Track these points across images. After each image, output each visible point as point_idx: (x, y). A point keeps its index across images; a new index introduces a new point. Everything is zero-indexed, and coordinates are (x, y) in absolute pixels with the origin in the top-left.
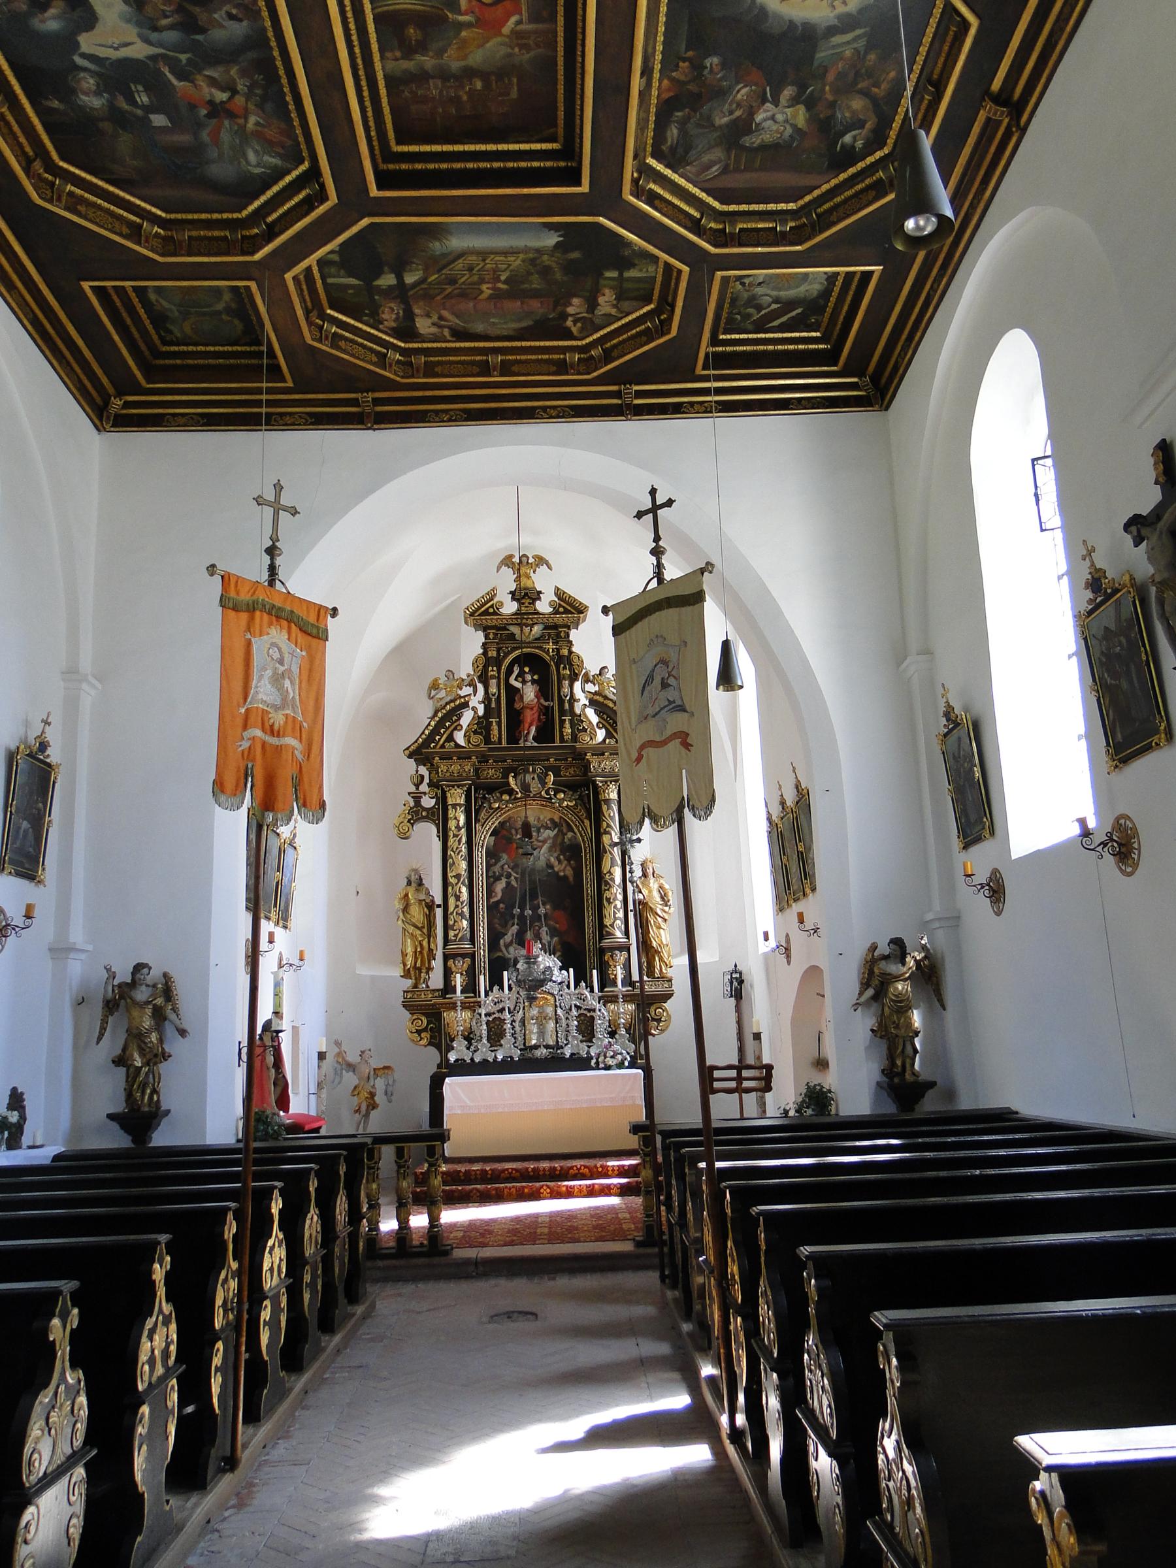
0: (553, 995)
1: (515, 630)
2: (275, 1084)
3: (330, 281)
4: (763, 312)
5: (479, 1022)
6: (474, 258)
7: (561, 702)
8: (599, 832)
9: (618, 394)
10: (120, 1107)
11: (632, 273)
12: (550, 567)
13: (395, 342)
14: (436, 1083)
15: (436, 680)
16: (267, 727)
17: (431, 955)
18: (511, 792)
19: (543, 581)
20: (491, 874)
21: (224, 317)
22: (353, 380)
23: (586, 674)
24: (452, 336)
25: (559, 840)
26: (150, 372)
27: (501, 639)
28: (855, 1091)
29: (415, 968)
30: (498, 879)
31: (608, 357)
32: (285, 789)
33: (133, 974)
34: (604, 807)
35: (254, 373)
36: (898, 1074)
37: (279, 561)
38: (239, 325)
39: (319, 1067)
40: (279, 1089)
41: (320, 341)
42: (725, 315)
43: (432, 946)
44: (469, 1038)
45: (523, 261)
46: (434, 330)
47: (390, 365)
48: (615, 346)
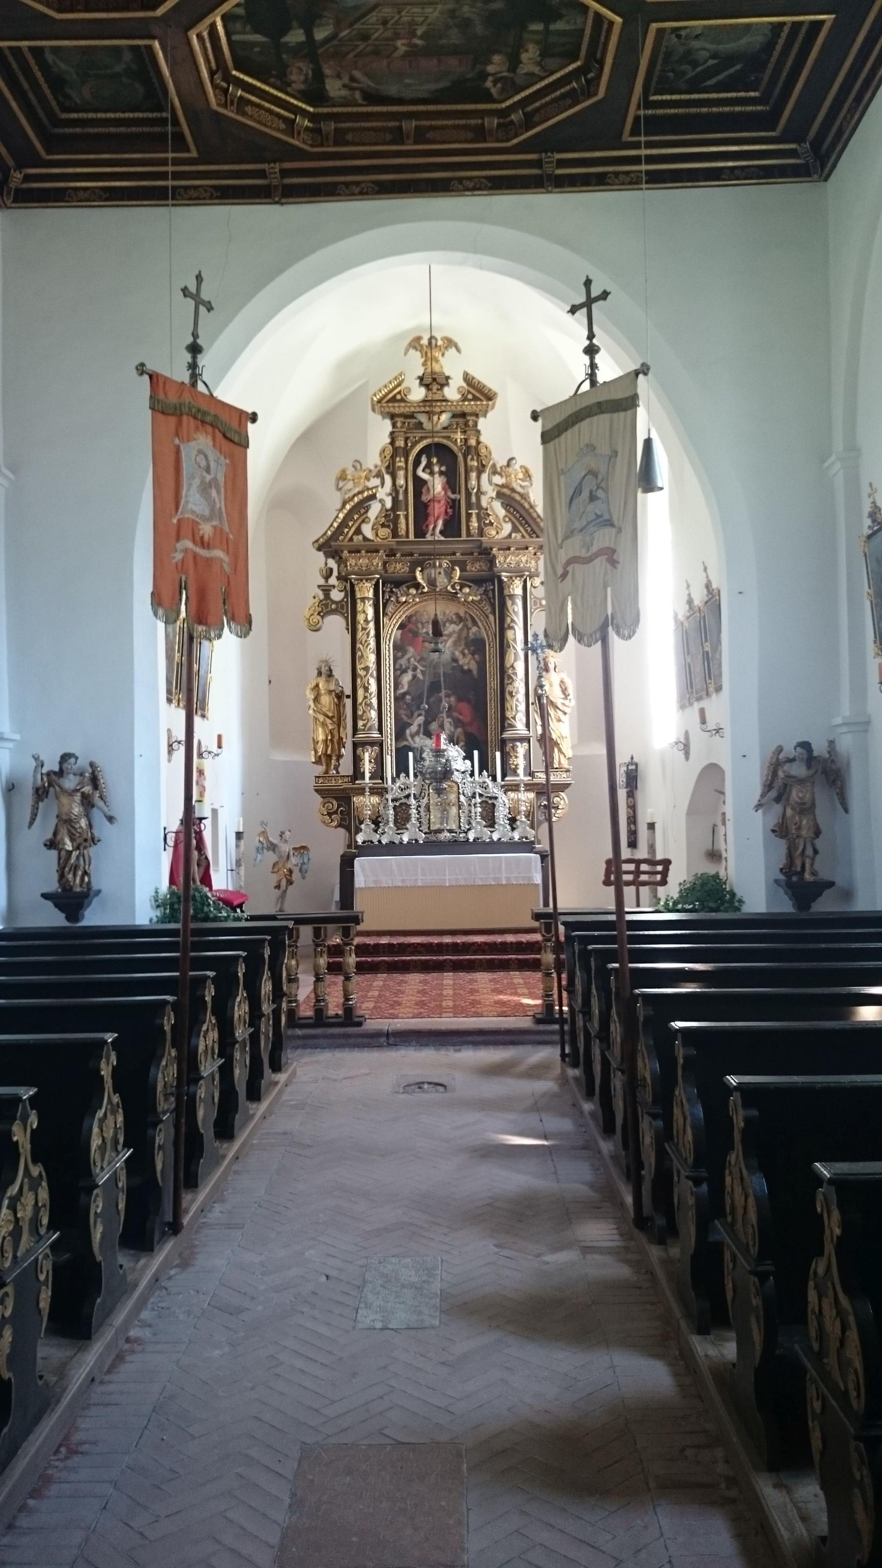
0: (456, 783)
1: (423, 418)
2: (198, 865)
3: (235, 38)
4: (699, 69)
5: (386, 807)
6: (390, 10)
7: (468, 494)
8: (503, 627)
9: (538, 164)
10: (53, 886)
11: (559, 26)
12: (458, 350)
13: (304, 106)
14: (347, 863)
15: (344, 471)
16: (198, 539)
17: (341, 743)
18: (418, 586)
19: (452, 366)
20: (397, 667)
21: (125, 80)
22: (258, 148)
23: (494, 466)
24: (364, 99)
25: (464, 634)
26: (52, 142)
27: (409, 429)
28: (754, 887)
29: (326, 754)
30: (404, 671)
31: (528, 123)
32: (215, 604)
33: (61, 763)
34: (509, 603)
35: (158, 141)
36: (797, 873)
37: (202, 360)
38: (140, 89)
39: (237, 846)
40: (202, 869)
41: (225, 106)
42: (657, 73)
43: (343, 735)
44: (376, 822)
45: (442, 13)
46: (344, 93)
47: (299, 133)
48: (537, 110)
